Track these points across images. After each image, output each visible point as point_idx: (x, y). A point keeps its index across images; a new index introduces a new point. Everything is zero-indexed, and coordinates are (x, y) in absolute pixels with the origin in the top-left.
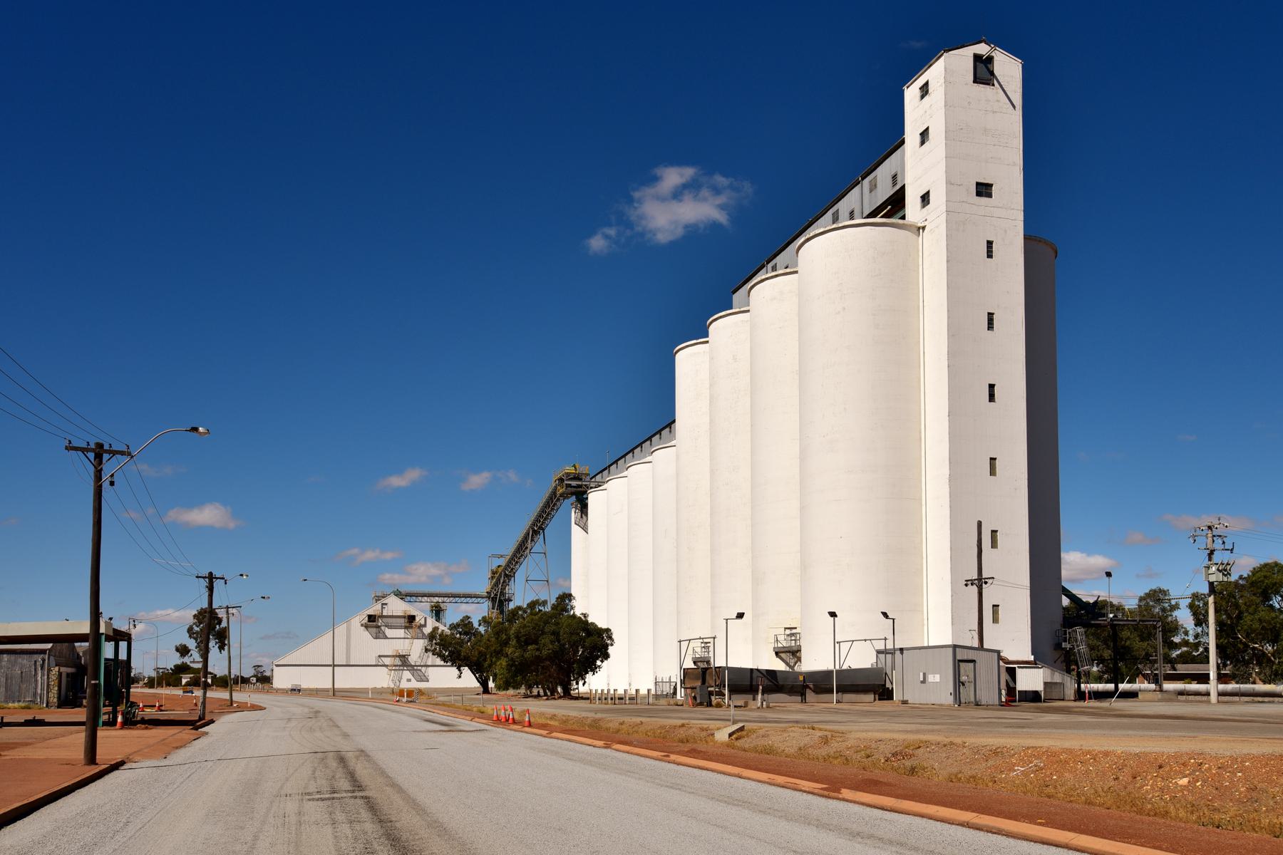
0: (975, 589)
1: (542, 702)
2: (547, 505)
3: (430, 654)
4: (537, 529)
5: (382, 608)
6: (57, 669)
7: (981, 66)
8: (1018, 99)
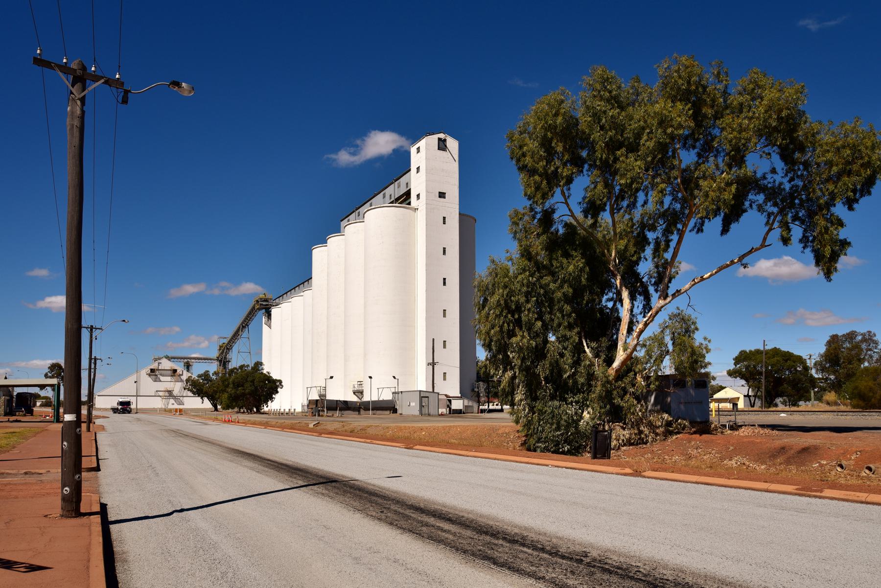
0: (431, 367)
1: (245, 415)
2: (250, 313)
3: (186, 390)
4: (244, 325)
5: (159, 365)
6: (4, 397)
7: (441, 143)
8: (457, 158)
